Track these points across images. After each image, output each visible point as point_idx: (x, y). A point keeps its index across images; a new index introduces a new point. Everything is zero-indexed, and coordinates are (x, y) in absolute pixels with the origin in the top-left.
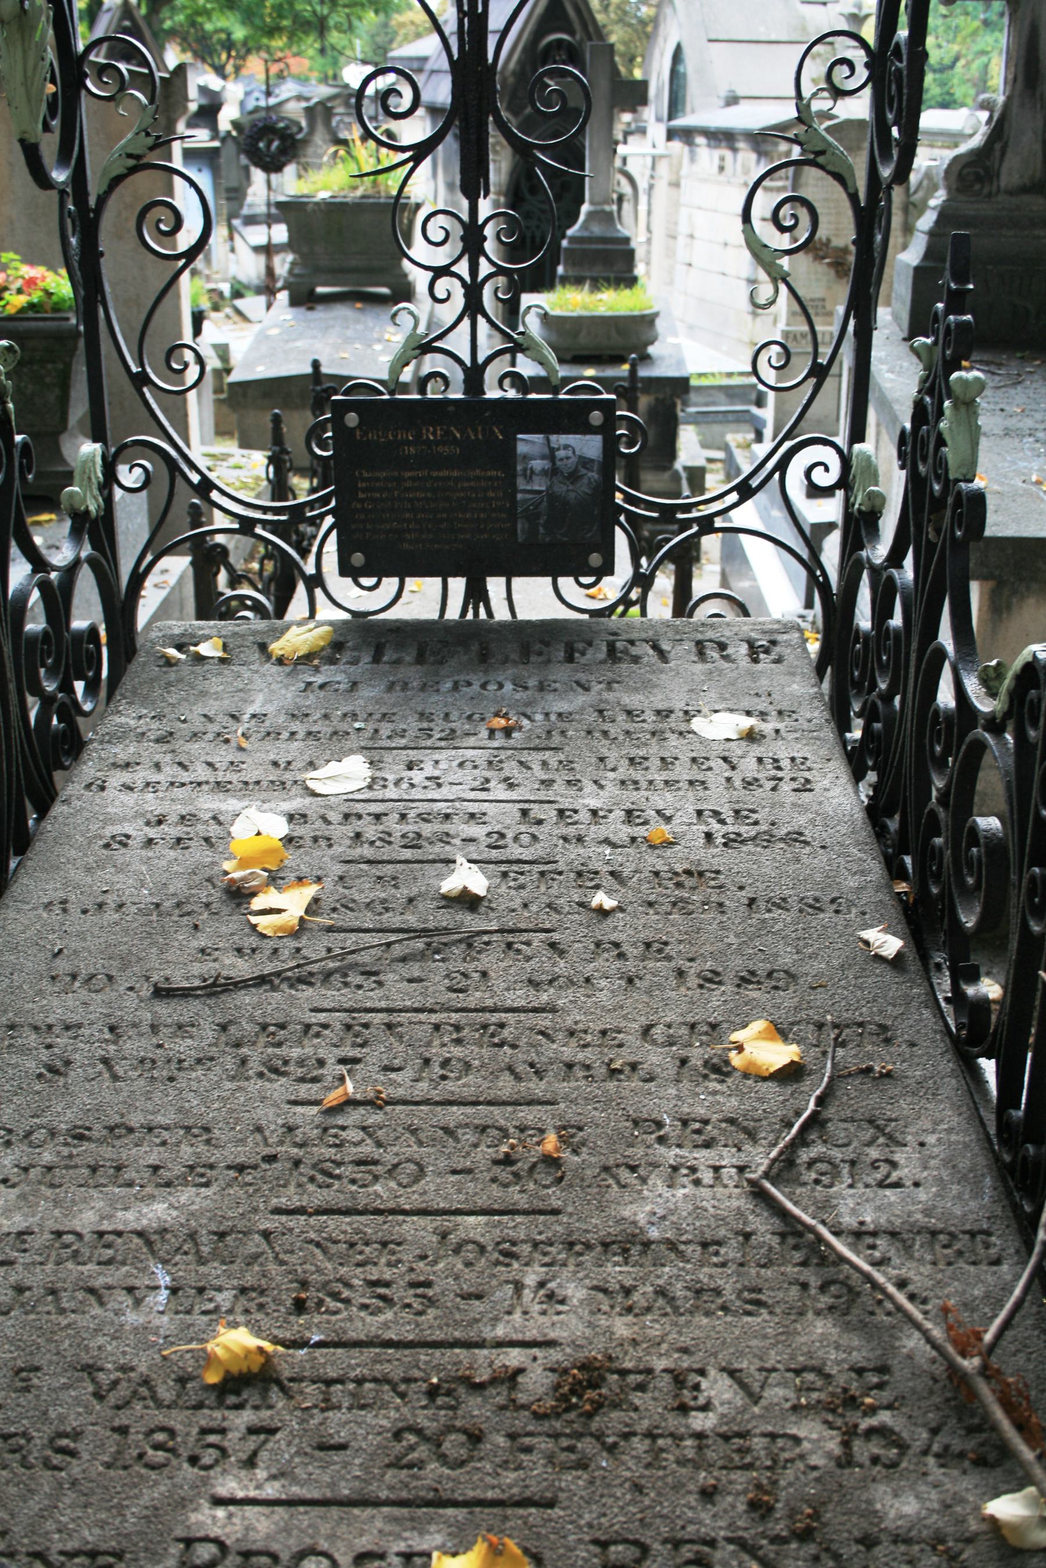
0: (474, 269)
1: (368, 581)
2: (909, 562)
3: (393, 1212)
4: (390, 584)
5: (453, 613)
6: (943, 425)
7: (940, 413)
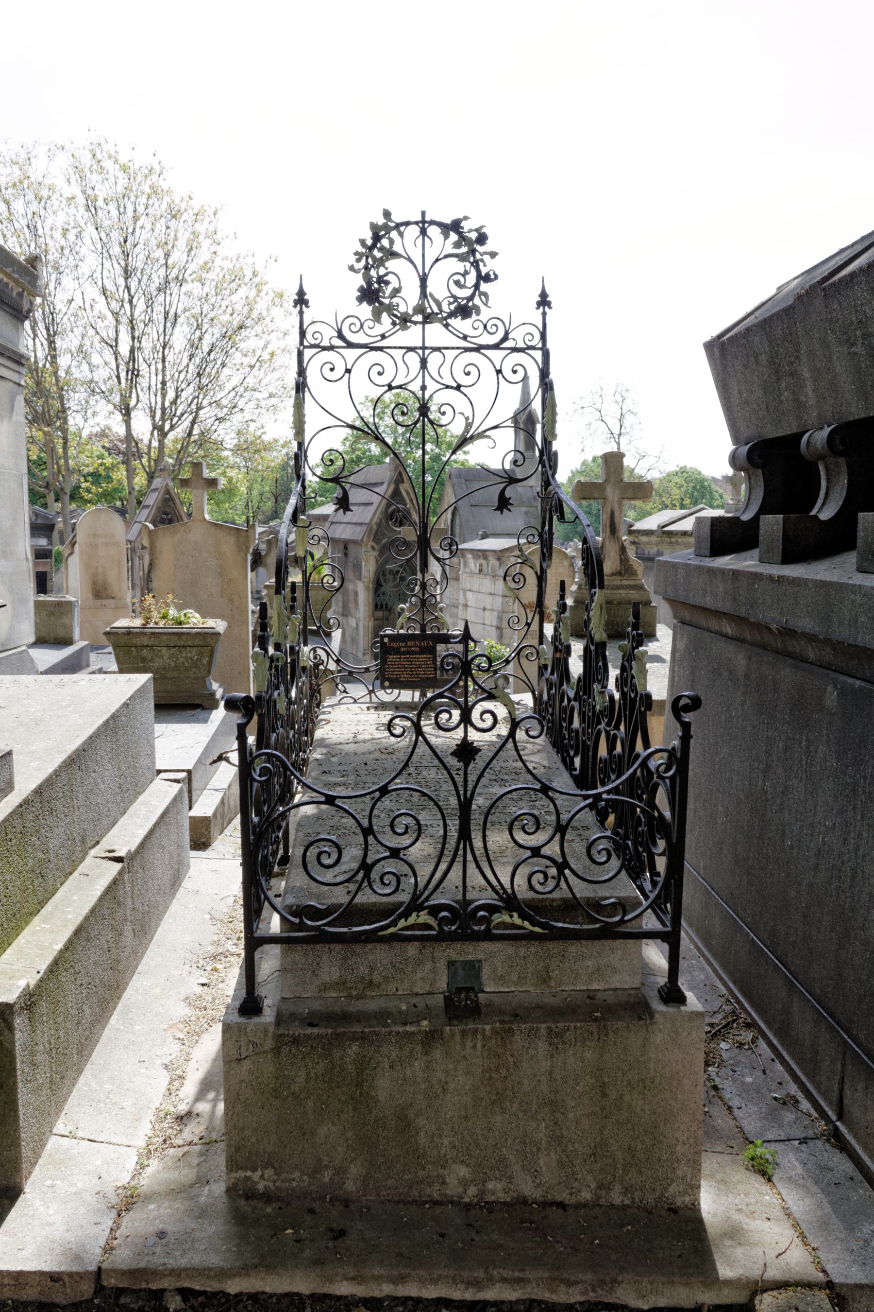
0: (423, 595)
1: (389, 691)
2: (622, 727)
3: (355, 524)
4: (396, 691)
5: (416, 699)
6: (633, 672)
7: (631, 668)
